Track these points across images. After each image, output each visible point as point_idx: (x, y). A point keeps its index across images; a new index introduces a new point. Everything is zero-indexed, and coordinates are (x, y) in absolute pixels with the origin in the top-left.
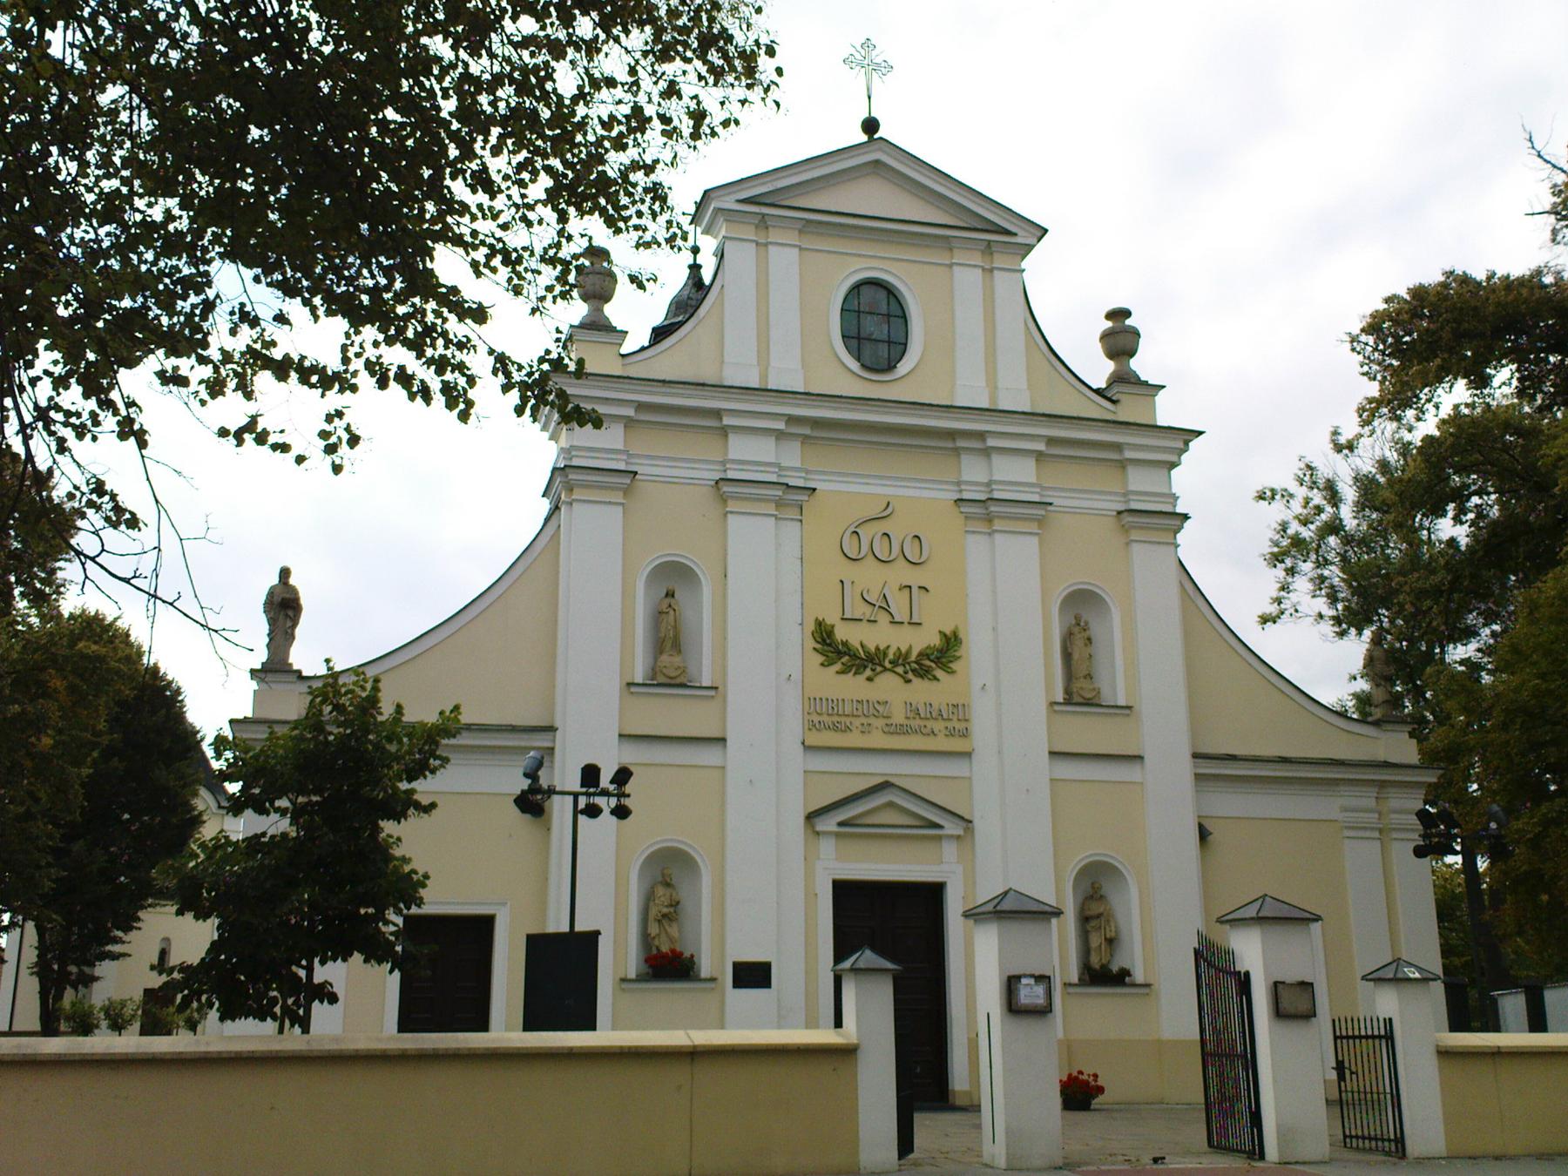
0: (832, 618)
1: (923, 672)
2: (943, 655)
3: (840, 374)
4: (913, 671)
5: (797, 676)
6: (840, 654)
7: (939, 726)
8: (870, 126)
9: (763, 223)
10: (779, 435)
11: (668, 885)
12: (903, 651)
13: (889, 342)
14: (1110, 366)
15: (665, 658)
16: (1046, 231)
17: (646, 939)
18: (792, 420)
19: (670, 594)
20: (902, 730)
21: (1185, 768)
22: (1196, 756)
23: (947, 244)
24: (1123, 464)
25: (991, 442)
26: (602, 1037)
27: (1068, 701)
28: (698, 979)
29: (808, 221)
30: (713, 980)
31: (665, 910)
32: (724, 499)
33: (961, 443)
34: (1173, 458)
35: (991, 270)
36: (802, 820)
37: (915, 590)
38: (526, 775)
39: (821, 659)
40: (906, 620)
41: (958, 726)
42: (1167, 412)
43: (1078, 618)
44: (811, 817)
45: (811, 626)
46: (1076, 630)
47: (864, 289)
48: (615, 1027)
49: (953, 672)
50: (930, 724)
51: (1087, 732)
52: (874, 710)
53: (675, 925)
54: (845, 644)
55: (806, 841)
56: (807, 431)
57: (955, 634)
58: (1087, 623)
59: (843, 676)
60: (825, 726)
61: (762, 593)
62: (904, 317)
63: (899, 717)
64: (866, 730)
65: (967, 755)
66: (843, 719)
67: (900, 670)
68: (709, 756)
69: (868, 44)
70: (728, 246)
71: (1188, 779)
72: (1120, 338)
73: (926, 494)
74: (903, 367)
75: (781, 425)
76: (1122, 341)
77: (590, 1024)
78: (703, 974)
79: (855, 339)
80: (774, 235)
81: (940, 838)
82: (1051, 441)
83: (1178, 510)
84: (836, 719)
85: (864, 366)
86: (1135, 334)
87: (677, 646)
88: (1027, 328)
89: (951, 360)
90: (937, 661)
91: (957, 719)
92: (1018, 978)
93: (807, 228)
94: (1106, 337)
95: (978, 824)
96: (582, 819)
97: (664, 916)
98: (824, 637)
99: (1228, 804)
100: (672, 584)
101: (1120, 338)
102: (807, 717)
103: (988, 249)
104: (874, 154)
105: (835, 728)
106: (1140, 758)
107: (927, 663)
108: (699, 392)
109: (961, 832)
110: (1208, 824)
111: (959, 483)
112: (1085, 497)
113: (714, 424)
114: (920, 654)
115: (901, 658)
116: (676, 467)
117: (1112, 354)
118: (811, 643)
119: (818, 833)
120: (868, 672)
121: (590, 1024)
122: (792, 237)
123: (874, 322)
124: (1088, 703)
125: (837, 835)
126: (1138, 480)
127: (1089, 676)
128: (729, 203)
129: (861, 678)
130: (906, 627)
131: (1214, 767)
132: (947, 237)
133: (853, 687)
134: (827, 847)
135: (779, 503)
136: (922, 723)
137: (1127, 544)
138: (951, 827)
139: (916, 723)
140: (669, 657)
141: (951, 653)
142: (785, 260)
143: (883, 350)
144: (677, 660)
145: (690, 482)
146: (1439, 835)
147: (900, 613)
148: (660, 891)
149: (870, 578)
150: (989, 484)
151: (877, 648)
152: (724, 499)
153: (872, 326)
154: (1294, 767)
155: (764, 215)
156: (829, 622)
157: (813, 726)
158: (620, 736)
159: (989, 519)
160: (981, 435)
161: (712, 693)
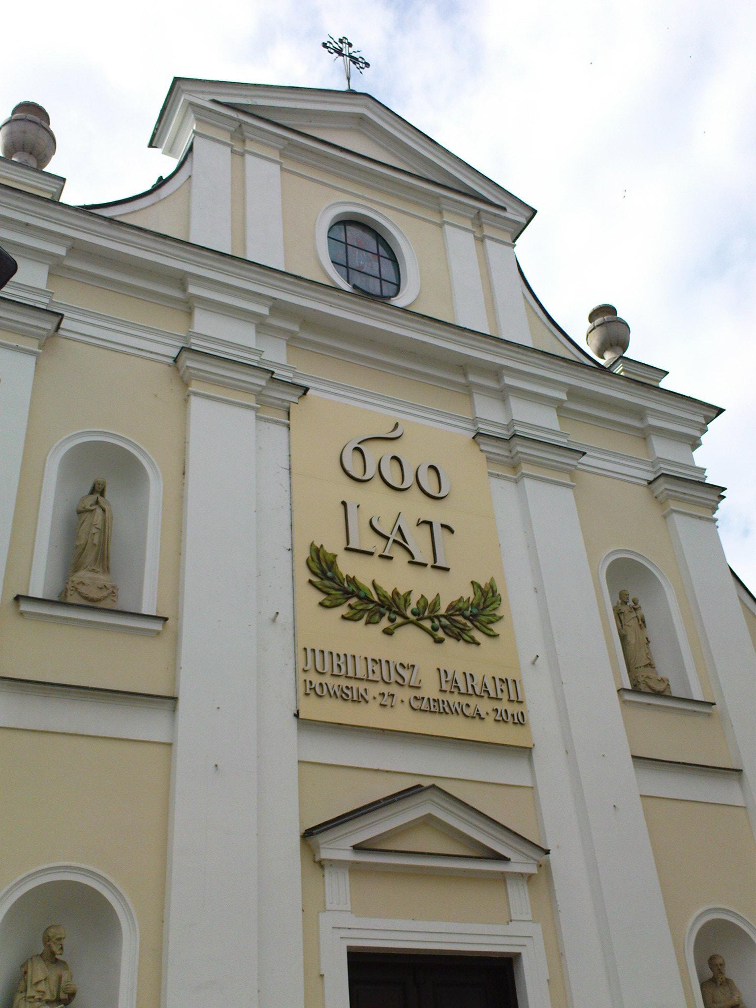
0: (334, 545)
1: (459, 634)
2: (474, 616)
4: (444, 628)
5: (286, 616)
6: (348, 594)
7: (485, 706)
9: (239, 134)
10: (262, 326)
11: (52, 958)
12: (430, 599)
15: (83, 575)
16: (534, 212)
18: (278, 308)
19: (98, 490)
27: (636, 689)
36: (297, 839)
37: (391, 541)
41: (513, 709)
44: (308, 834)
45: (304, 553)
49: (495, 636)
50: (473, 701)
52: (400, 675)
54: (352, 580)
55: (303, 876)
57: (492, 587)
58: (635, 602)
63: (430, 690)
64: (387, 702)
66: (354, 684)
68: (147, 725)
70: (199, 143)
81: (502, 878)
84: (344, 683)
87: (103, 560)
88: (525, 298)
90: (473, 618)
91: (505, 698)
98: (322, 567)
102: (302, 676)
106: (740, 771)
108: (158, 245)
109: (532, 869)
112: (614, 462)
114: (451, 607)
118: (305, 575)
119: (321, 864)
120: (385, 623)
125: (354, 869)
127: (650, 665)
128: (203, 100)
129: (376, 630)
133: (364, 640)
134: (337, 888)
136: (464, 700)
137: (665, 517)
139: (454, 699)
141: (487, 611)
144: (102, 578)
145: (138, 354)
147: (423, 554)
148: (39, 971)
151: (395, 593)
156: (329, 549)
161: (157, 626)
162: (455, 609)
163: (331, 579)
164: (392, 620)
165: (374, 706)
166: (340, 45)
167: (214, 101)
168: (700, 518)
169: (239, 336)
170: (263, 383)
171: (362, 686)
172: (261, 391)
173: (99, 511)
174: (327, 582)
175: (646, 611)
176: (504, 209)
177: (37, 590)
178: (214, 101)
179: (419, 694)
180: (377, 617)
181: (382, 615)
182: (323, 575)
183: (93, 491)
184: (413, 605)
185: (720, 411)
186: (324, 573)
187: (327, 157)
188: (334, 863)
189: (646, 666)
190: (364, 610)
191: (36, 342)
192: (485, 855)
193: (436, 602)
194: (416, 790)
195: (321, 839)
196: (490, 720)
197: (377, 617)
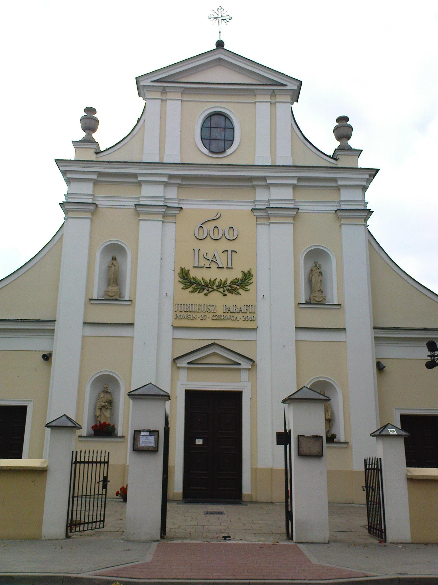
0: (188, 266)
2: (245, 281)
3: (199, 154)
6: (192, 283)
7: (240, 316)
8: (220, 44)
9: (164, 91)
10: (166, 184)
13: (225, 140)
14: (337, 144)
17: (96, 417)
18: (171, 176)
19: (114, 259)
20: (221, 319)
21: (367, 335)
22: (375, 328)
23: (253, 93)
24: (338, 188)
28: (116, 436)
29: (185, 88)
30: (122, 437)
31: (103, 404)
32: (138, 214)
33: (254, 183)
34: (364, 183)
36: (170, 361)
37: (230, 252)
39: (182, 286)
42: (363, 162)
43: (316, 263)
44: (175, 360)
45: (178, 271)
46: (314, 269)
47: (213, 117)
50: (235, 315)
52: (210, 309)
56: (179, 181)
57: (249, 272)
58: (320, 265)
59: (193, 294)
60: (247, 321)
61: (155, 256)
62: (233, 128)
63: (220, 312)
65: (254, 329)
67: (221, 290)
71: (291, 335)
72: (343, 129)
74: (229, 151)
76: (344, 131)
77: (19, 456)
78: (119, 434)
81: (240, 369)
82: (299, 179)
83: (368, 208)
85: (210, 151)
86: (97, 121)
91: (250, 313)
92: (139, 432)
93: (185, 91)
95: (258, 362)
97: (103, 406)
99: (392, 352)
100: (115, 253)
101: (343, 129)
103: (273, 94)
106: (345, 329)
107: (235, 286)
109: (250, 367)
110: (383, 363)
112: (317, 206)
114: (231, 282)
115: (222, 285)
116: (116, 201)
117: (338, 138)
119: (179, 368)
120: (205, 292)
122: (178, 96)
123: (217, 131)
124: (318, 303)
125: (188, 368)
126: (346, 195)
127: (320, 291)
128: (147, 82)
130: (225, 270)
131: (384, 333)
133: (199, 298)
134: (183, 374)
135: (164, 215)
136: (232, 315)
138: (244, 364)
139: (228, 315)
141: (246, 281)
142: (174, 106)
143: (222, 144)
145: (123, 207)
148: (102, 395)
149: (210, 248)
150: (268, 201)
152: (138, 214)
153: (216, 133)
154: (431, 332)
155: (164, 87)
156: (187, 269)
158: (84, 323)
159: (268, 218)
160: (264, 178)
162: (233, 283)
163: (186, 279)
164: (208, 290)
165: (199, 320)
166: (217, 13)
167: (152, 81)
168: (356, 224)
169: (157, 191)
170: (164, 210)
171: (194, 314)
172: (165, 212)
173: (113, 266)
174: (185, 281)
175: (323, 269)
176: (286, 85)
177: (95, 297)
178: (152, 81)
179: (215, 314)
180: (202, 290)
181: (204, 289)
182: (184, 278)
183: (113, 259)
184: (217, 283)
186: (184, 277)
187: (201, 88)
188: (182, 368)
189: (318, 291)
190: (198, 288)
191: (90, 214)
192: (232, 363)
193: (226, 281)
195: (177, 361)
196: (241, 321)
197: (202, 290)
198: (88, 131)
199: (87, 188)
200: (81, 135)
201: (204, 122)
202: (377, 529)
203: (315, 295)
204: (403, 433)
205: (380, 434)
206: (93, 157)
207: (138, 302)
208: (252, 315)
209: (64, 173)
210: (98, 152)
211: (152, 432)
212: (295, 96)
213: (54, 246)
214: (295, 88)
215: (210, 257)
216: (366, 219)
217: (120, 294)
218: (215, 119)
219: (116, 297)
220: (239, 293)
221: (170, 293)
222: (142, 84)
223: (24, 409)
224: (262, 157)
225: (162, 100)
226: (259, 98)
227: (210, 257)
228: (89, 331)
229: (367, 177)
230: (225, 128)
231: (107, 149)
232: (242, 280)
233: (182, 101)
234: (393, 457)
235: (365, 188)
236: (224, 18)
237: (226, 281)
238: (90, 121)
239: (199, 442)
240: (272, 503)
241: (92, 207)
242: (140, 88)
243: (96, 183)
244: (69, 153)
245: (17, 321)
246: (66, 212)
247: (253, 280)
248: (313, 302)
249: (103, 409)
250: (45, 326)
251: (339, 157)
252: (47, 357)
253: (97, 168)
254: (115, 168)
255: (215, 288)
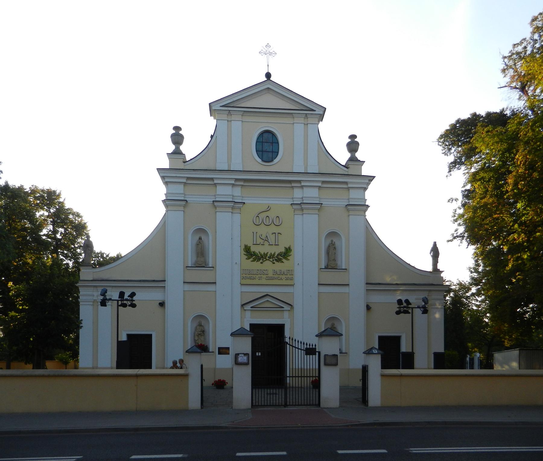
0: (250, 244)
1: (279, 260)
2: (286, 253)
3: (255, 163)
4: (276, 260)
5: (239, 262)
7: (283, 277)
8: (268, 75)
10: (233, 185)
14: (349, 155)
17: (195, 341)
18: (236, 180)
20: (272, 279)
24: (348, 189)
25: (303, 184)
26: (153, 371)
29: (244, 111)
30: (213, 352)
33: (293, 185)
34: (365, 186)
35: (307, 124)
38: (101, 295)
40: (274, 244)
42: (365, 171)
43: (332, 241)
44: (243, 305)
45: (243, 247)
48: (157, 368)
50: (280, 276)
51: (331, 276)
53: (203, 337)
57: (289, 248)
60: (247, 277)
61: (228, 236)
65: (293, 285)
67: (271, 260)
68: (211, 288)
69: (268, 46)
72: (353, 145)
73: (282, 202)
74: (276, 161)
75: (233, 182)
79: (260, 152)
80: (233, 117)
82: (323, 182)
85: (263, 161)
86: (357, 144)
89: (292, 157)
92: (238, 354)
94: (348, 145)
95: (295, 306)
96: (120, 308)
99: (376, 298)
101: (353, 145)
104: (268, 87)
105: (250, 278)
110: (370, 305)
111: (293, 198)
112: (334, 201)
113: (212, 183)
114: (278, 255)
115: (272, 256)
116: (200, 196)
118: (243, 252)
120: (261, 261)
121: (150, 367)
122: (239, 117)
123: (267, 146)
128: (217, 107)
131: (372, 286)
132: (292, 113)
133: (257, 265)
134: (248, 314)
135: (233, 208)
138: (286, 307)
140: (201, 259)
146: (405, 307)
148: (198, 327)
149: (263, 230)
150: (302, 198)
153: (267, 147)
155: (229, 111)
157: (243, 278)
159: (302, 210)
160: (299, 182)
161: (212, 269)
162: (279, 254)
181: (260, 259)
182: (247, 252)
184: (268, 255)
185: (374, 177)
193: (274, 254)
194: (267, 295)
195: (244, 306)
198: (177, 145)
199: (180, 189)
200: (172, 148)
201: (258, 139)
202: (364, 399)
203: (331, 261)
204: (381, 352)
205: (369, 352)
206: (182, 166)
207: (218, 268)
208: (291, 276)
209: (163, 178)
210: (185, 162)
211: (245, 354)
212: (321, 117)
213: (162, 230)
214: (322, 113)
215: (263, 237)
216: (365, 211)
217: (205, 262)
218: (265, 135)
219: (204, 265)
220: (283, 262)
221: (238, 262)
222: (213, 108)
223: (150, 336)
224: (299, 167)
225: (228, 121)
226: (296, 120)
227: (263, 237)
228: (187, 287)
229: (367, 181)
230: (272, 143)
231: (191, 159)
232: (284, 253)
233: (242, 121)
234: (375, 363)
235: (365, 189)
236: (270, 54)
237: (274, 254)
238: (177, 138)
239: (258, 354)
240: (202, 366)
241: (184, 203)
242: (212, 111)
243: (185, 184)
244: (166, 164)
245: (140, 281)
246: (166, 206)
247: (292, 253)
248: (330, 267)
249: (200, 336)
250: (159, 283)
251: (350, 166)
252: (162, 304)
253: (187, 174)
254: (198, 174)
255: (267, 258)
